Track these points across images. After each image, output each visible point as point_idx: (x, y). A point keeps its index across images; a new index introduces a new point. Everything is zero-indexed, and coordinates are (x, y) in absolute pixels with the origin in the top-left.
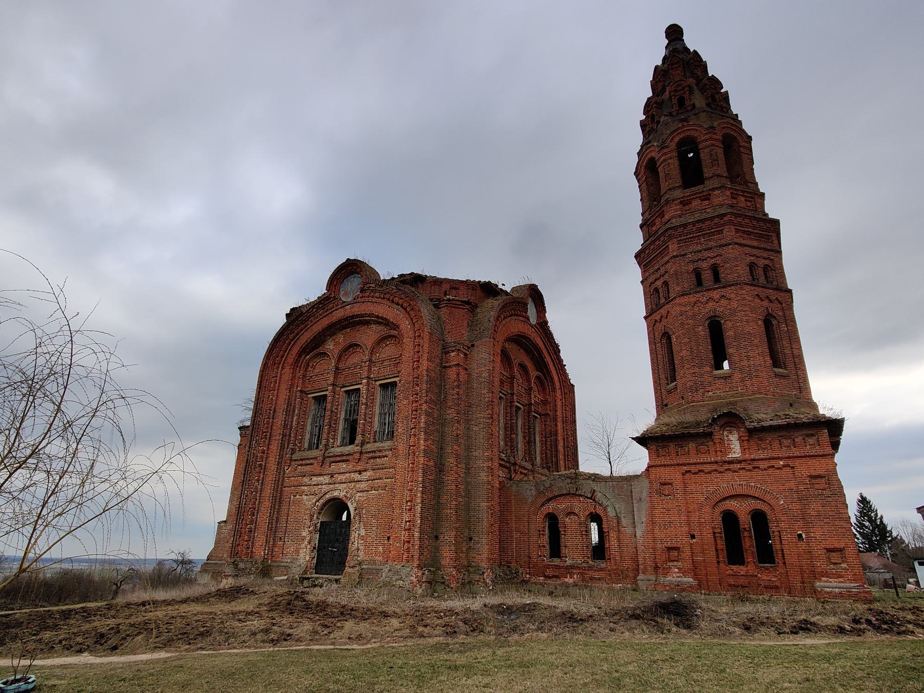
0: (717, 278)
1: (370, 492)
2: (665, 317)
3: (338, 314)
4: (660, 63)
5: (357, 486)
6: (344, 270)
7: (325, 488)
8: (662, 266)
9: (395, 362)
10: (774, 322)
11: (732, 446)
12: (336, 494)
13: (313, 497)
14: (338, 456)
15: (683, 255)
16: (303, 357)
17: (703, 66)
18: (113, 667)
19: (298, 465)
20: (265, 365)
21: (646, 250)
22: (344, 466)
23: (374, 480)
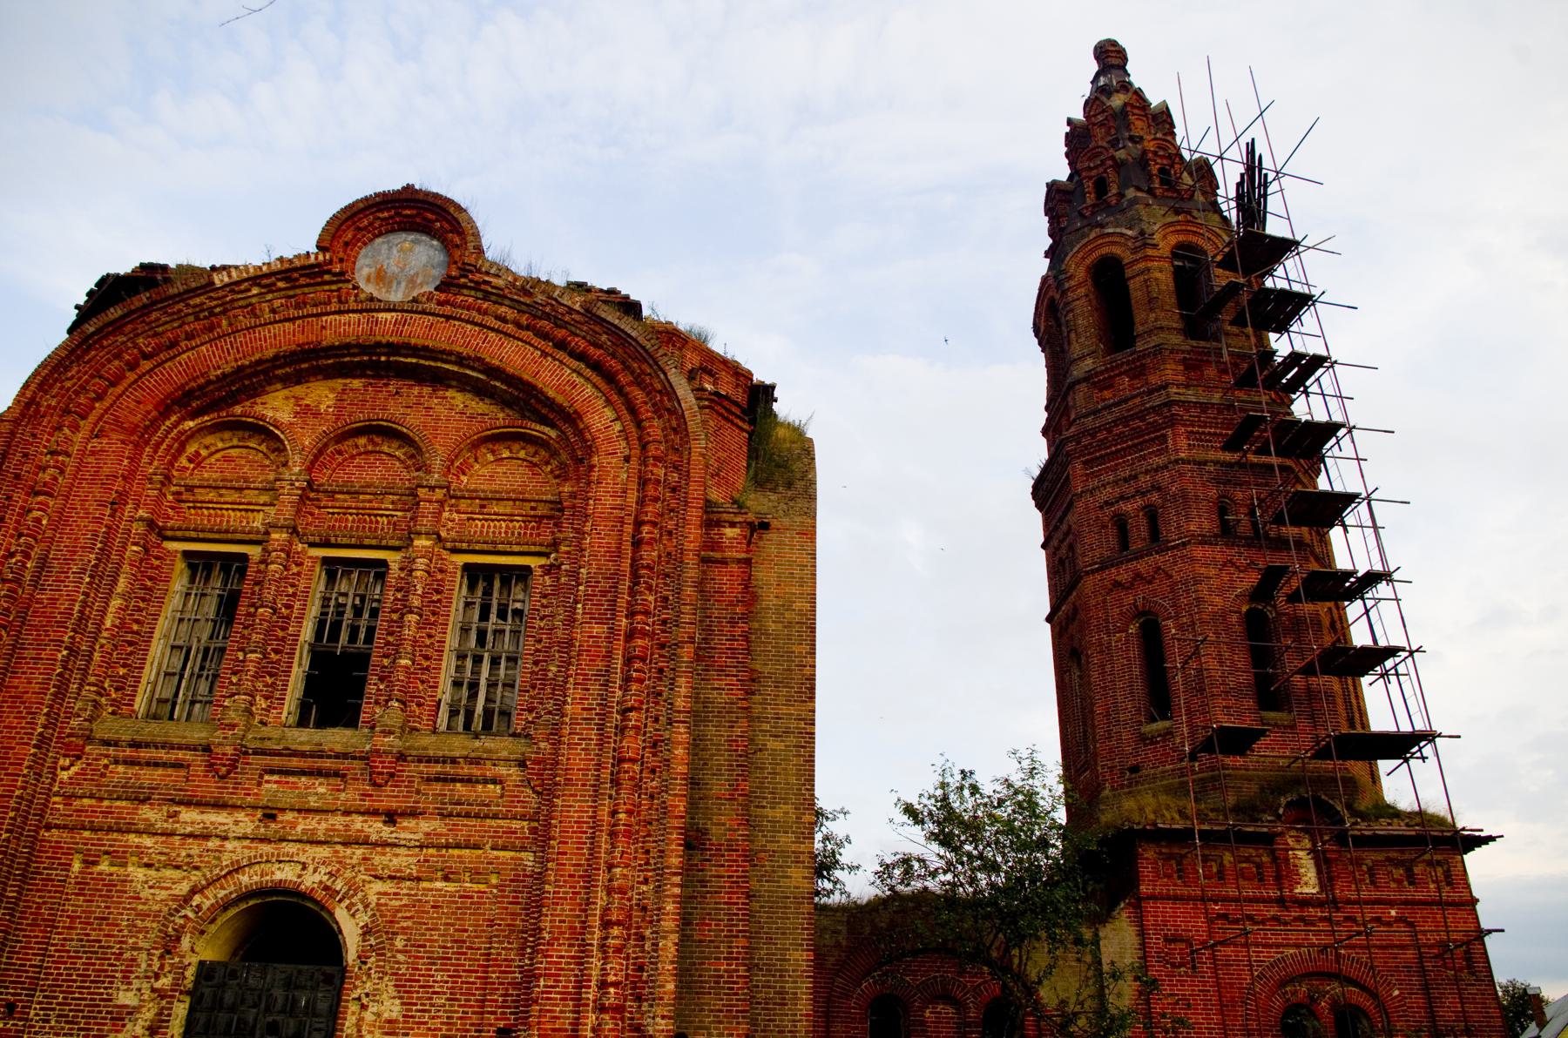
1: (425, 884)
3: (341, 327)
5: (377, 859)
6: (388, 210)
7: (234, 850)
8: (1147, 472)
9: (532, 513)
11: (1302, 870)
12: (285, 874)
13: (177, 874)
14: (302, 755)
15: (1199, 463)
16: (174, 418)
19: (116, 762)
20: (28, 405)
22: (322, 790)
23: (447, 846)
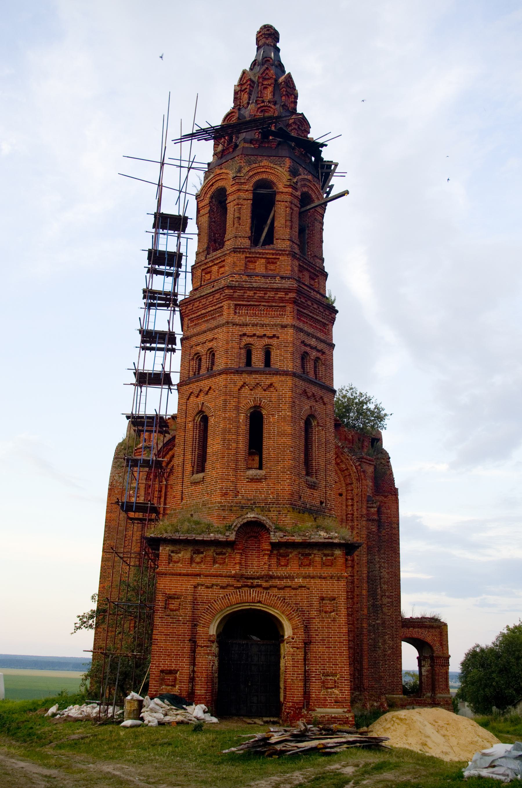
0: (267, 362)
2: (196, 395)
4: (247, 67)
10: (314, 423)
17: (297, 99)
18: (251, 733)
21: (190, 304)
